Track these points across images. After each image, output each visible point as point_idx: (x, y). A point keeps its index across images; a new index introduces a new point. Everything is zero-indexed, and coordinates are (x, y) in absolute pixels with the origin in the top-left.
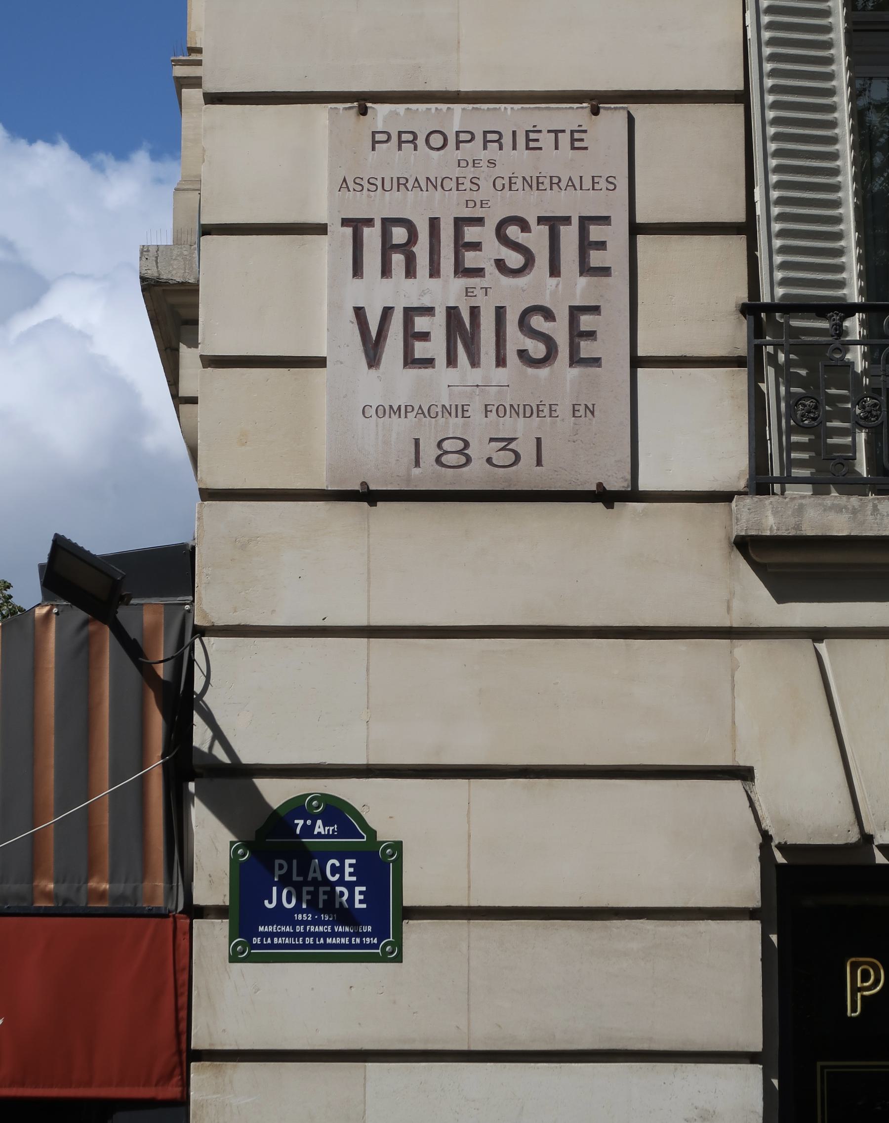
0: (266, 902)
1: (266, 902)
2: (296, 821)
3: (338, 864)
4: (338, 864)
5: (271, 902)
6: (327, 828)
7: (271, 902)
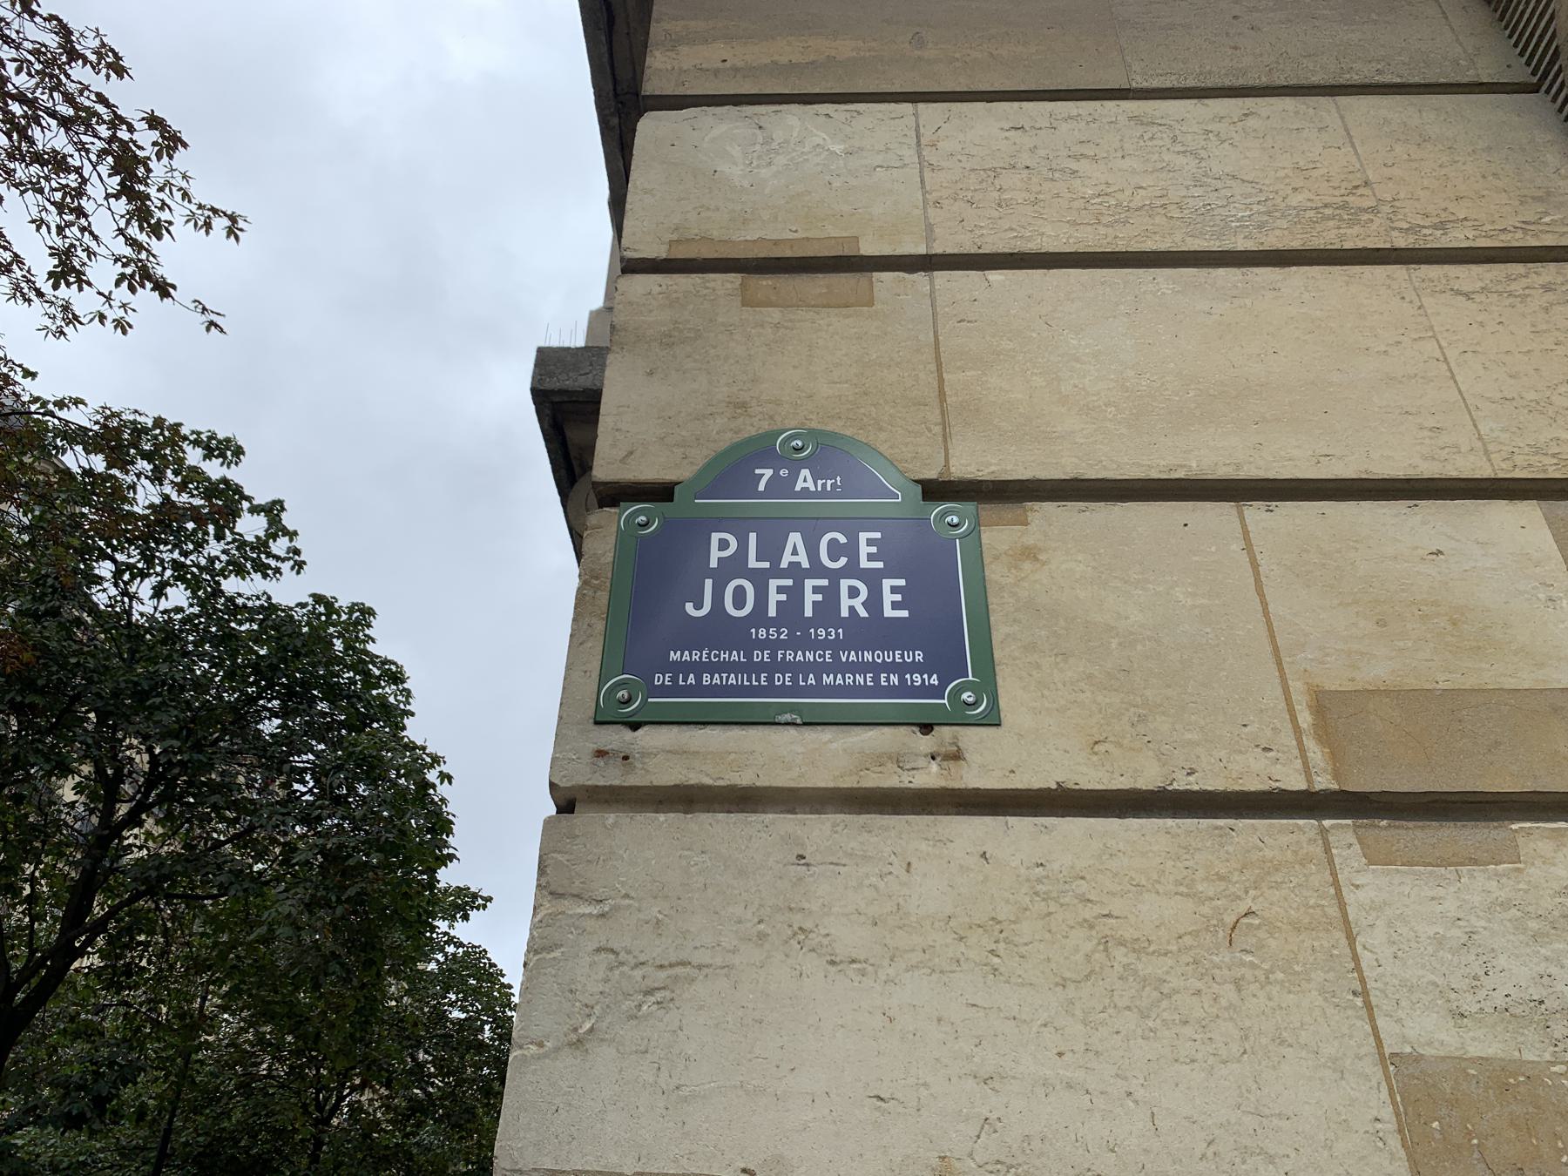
0: (689, 607)
1: (689, 607)
2: (758, 471)
3: (842, 539)
4: (842, 539)
5: (698, 606)
6: (820, 482)
7: (698, 606)
